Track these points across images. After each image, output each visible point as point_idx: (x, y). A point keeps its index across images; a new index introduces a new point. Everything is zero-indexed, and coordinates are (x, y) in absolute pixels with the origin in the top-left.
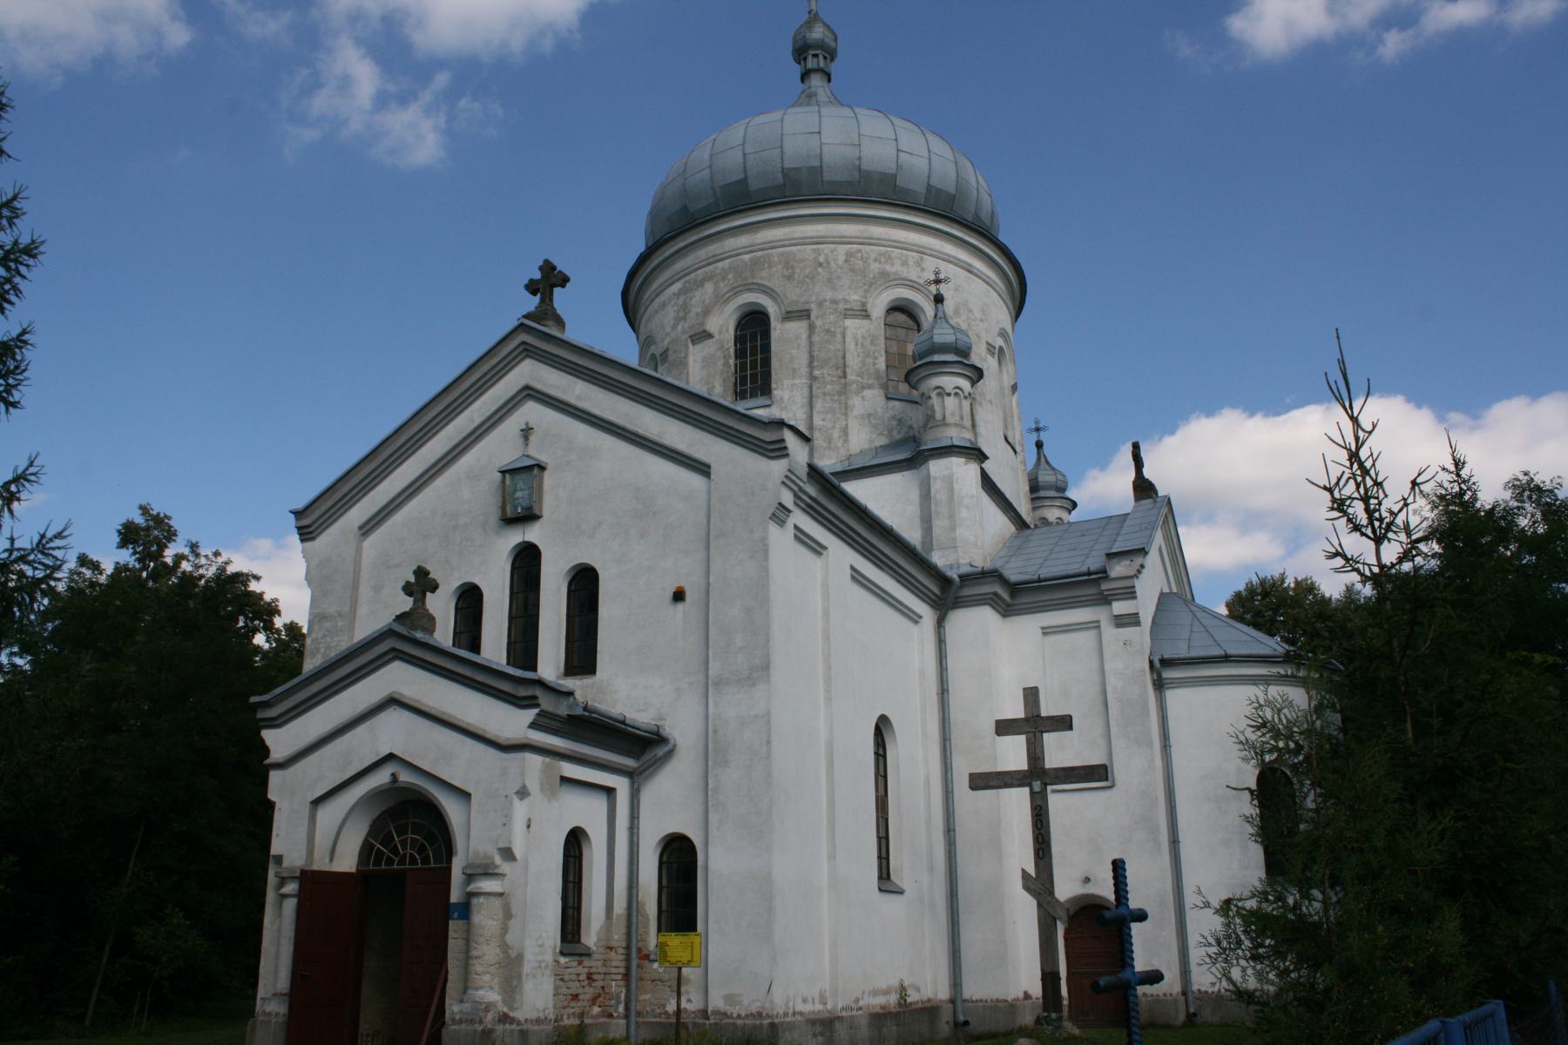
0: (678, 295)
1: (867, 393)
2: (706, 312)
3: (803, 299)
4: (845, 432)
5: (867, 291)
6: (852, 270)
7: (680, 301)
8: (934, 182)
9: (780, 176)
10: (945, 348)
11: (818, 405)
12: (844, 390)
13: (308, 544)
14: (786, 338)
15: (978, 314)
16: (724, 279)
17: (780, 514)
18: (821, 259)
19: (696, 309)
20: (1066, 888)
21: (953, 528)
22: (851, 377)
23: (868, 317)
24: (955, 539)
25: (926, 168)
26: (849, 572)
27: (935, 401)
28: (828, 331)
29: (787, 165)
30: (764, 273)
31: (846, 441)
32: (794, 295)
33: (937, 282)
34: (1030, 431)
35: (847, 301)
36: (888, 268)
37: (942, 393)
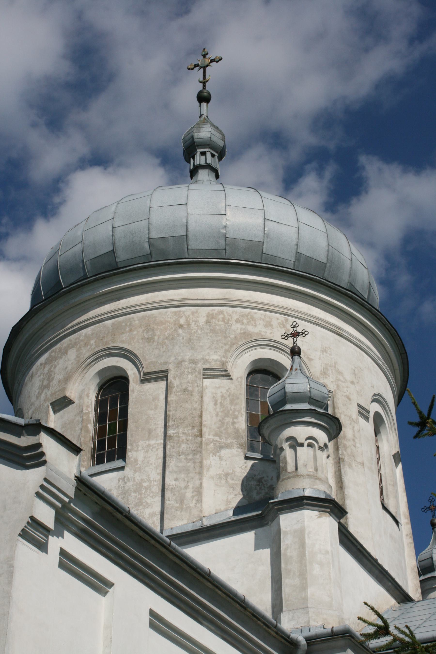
1: (224, 452)
2: (67, 379)
3: (162, 360)
4: (199, 492)
5: (227, 351)
6: (213, 331)
7: (46, 371)
9: (147, 245)
10: (299, 398)
11: (171, 464)
12: (198, 450)
14: (144, 398)
15: (348, 376)
16: (86, 344)
17: (35, 533)
18: (182, 321)
19: (58, 377)
21: (304, 587)
22: (208, 436)
23: (228, 376)
24: (305, 599)
25: (295, 236)
26: (147, 618)
27: (288, 453)
28: (185, 390)
29: (154, 235)
30: (125, 337)
31: (199, 501)
32: (151, 360)
33: (295, 335)
35: (206, 361)
36: (250, 328)
37: (295, 444)
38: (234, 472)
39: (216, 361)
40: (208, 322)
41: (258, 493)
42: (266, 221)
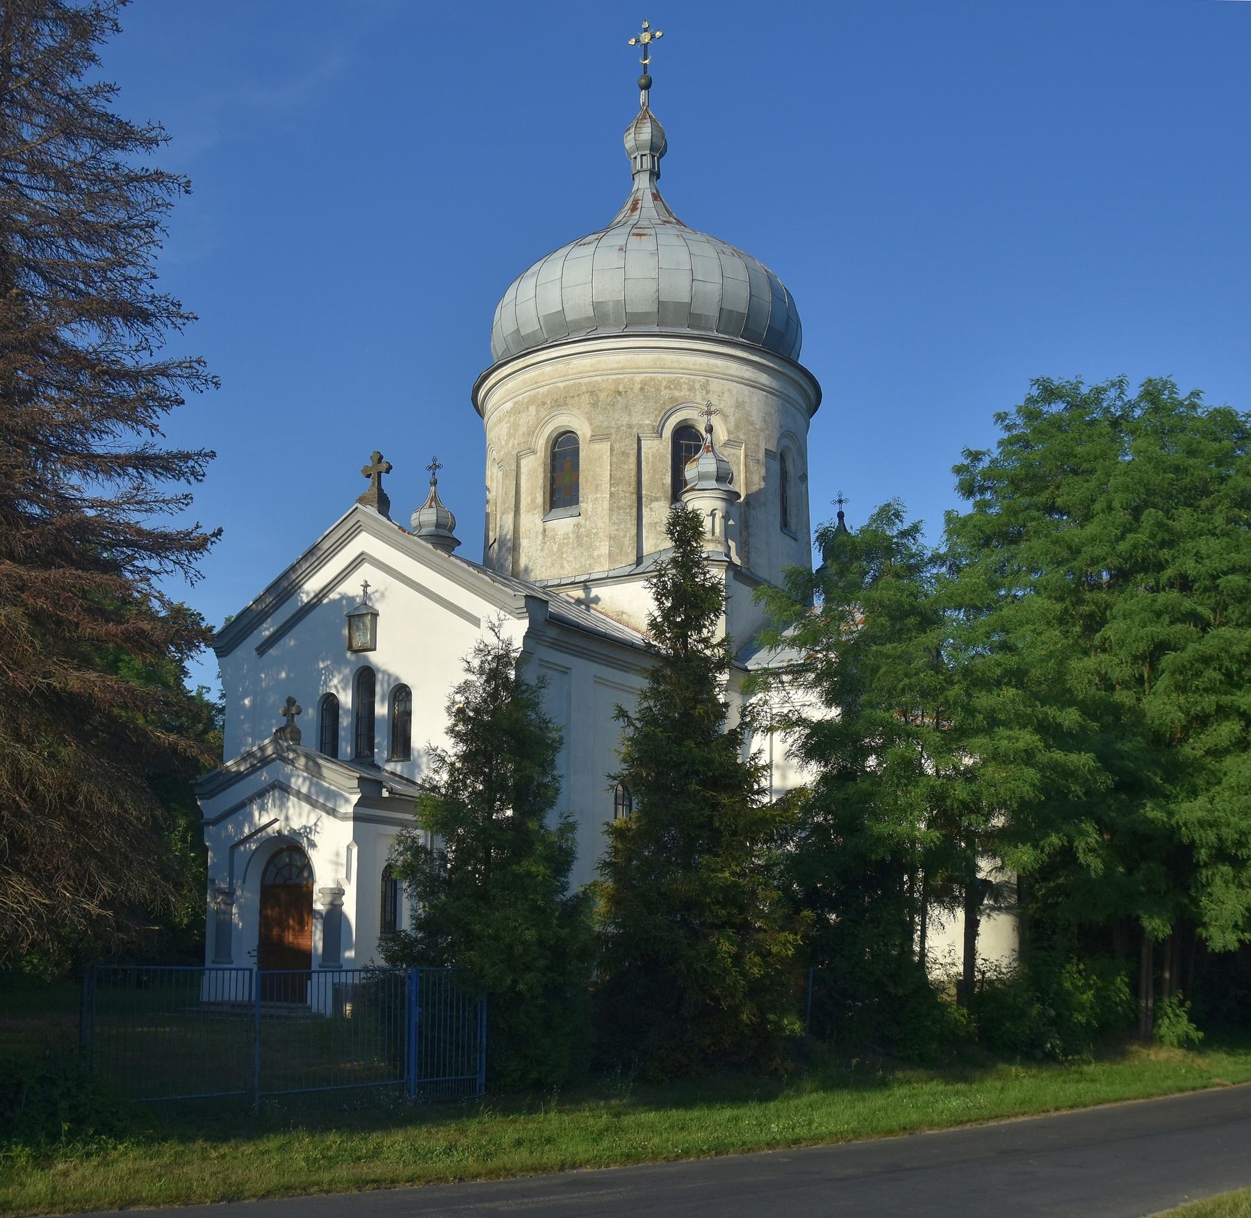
0: (510, 413)
7: (512, 419)
8: (727, 306)
18: (621, 389)
34: (834, 502)
36: (677, 393)
40: (642, 389)
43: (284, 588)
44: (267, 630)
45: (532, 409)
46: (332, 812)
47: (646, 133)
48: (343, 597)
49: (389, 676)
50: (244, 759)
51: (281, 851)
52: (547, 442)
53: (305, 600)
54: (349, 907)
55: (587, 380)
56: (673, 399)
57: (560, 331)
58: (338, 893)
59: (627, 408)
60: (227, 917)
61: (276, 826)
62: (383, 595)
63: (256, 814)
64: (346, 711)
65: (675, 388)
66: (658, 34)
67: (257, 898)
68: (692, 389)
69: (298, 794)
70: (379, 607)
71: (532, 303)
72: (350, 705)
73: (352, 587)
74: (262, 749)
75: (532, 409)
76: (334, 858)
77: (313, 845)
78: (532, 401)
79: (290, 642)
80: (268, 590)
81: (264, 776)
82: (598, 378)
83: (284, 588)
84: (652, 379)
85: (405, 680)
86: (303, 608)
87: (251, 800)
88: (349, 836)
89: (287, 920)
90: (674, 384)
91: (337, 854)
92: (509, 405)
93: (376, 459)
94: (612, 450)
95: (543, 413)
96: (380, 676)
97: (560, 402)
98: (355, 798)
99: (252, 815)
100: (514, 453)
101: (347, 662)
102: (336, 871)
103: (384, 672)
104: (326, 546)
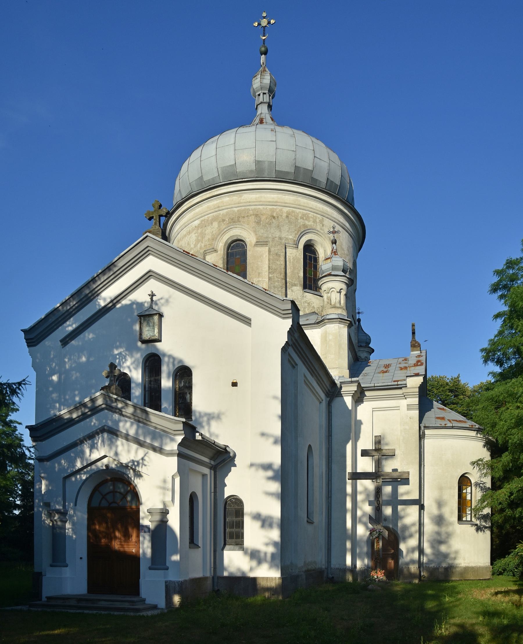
0: (197, 227)
7: (199, 231)
13: (33, 348)
18: (275, 215)
20: (375, 434)
38: (298, 298)
39: (291, 239)
40: (287, 217)
41: (308, 310)
42: (316, 158)
43: (85, 295)
44: (70, 326)
45: (215, 224)
46: (159, 450)
47: (267, 80)
48: (133, 303)
49: (174, 359)
50: (76, 409)
51: (105, 482)
52: (225, 245)
53: (102, 304)
54: (174, 521)
55: (253, 207)
56: (304, 226)
57: (232, 178)
58: (165, 512)
59: (278, 227)
60: (63, 531)
61: (105, 461)
62: (167, 301)
63: (87, 451)
64: (137, 385)
65: (306, 219)
66: (272, 21)
67: (86, 516)
68: (315, 221)
69: (127, 437)
70: (164, 310)
71: (213, 159)
72: (140, 380)
73: (141, 296)
74: (93, 400)
75: (215, 224)
76: (162, 485)
77: (139, 475)
78: (214, 219)
79: (89, 335)
80: (72, 296)
81: (94, 422)
82: (261, 207)
83: (85, 295)
84: (293, 212)
85: (188, 362)
86: (100, 310)
87: (81, 442)
88: (175, 470)
89: (114, 533)
90: (305, 217)
91: (165, 481)
92: (197, 223)
93: (157, 206)
94: (269, 251)
95: (223, 226)
96: (166, 359)
97: (235, 220)
98: (179, 439)
99: (83, 452)
100: (202, 251)
101: (138, 349)
102: (164, 494)
103: (170, 356)
104: (121, 264)
